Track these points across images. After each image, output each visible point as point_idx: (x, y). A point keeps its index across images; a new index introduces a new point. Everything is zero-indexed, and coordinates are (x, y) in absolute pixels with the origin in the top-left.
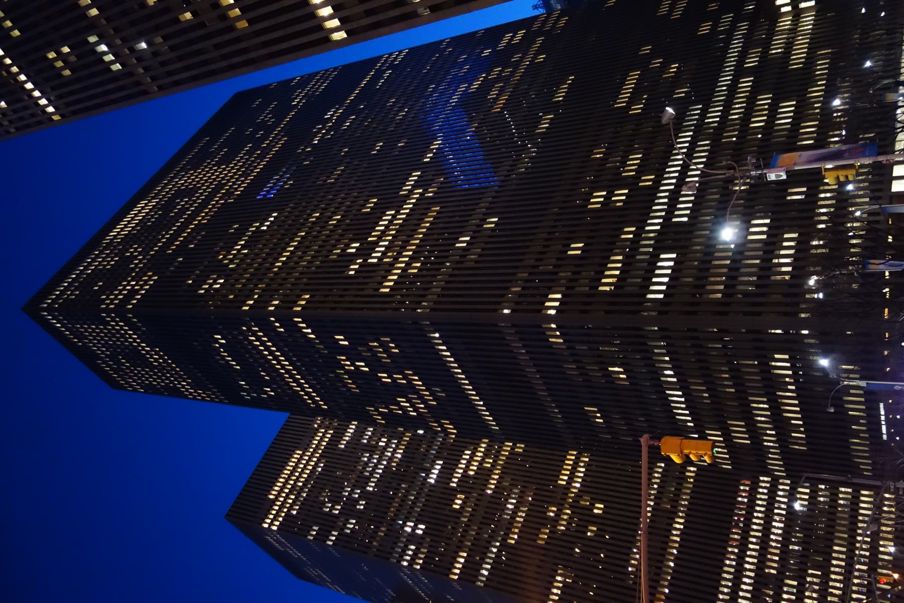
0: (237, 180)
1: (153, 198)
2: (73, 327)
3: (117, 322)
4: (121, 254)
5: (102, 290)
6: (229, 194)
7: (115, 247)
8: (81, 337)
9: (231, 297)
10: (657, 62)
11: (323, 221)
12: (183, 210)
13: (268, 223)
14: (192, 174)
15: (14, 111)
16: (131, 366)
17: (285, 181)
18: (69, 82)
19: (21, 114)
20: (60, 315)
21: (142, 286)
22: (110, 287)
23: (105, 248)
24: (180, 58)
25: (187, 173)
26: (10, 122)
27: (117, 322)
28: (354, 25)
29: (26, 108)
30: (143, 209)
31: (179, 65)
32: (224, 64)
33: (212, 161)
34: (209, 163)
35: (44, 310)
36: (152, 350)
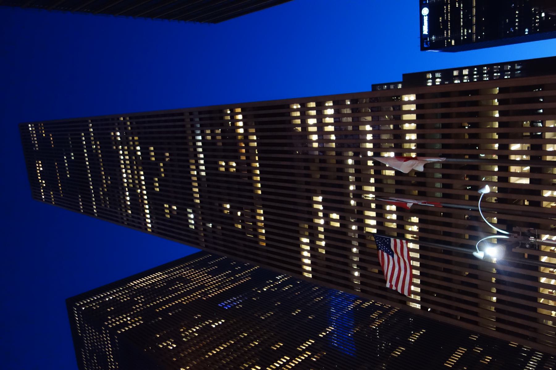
0: (214, 288)
1: (166, 274)
2: (84, 324)
3: (107, 336)
4: (132, 297)
5: (110, 314)
6: (205, 294)
7: (132, 291)
8: (83, 331)
9: (175, 359)
10: (478, 350)
11: (247, 340)
12: (177, 290)
13: (217, 324)
14: (192, 271)
15: (133, 217)
16: (97, 363)
17: (237, 303)
18: (166, 220)
19: (134, 220)
20: (81, 314)
21: (132, 323)
22: (116, 314)
23: (127, 289)
24: (224, 240)
25: (190, 269)
26: (128, 220)
27: (107, 336)
28: (318, 275)
29: (139, 218)
30: (158, 277)
31: (222, 243)
32: (244, 254)
33: (206, 269)
34: (204, 270)
35: (76, 306)
36: (113, 362)
